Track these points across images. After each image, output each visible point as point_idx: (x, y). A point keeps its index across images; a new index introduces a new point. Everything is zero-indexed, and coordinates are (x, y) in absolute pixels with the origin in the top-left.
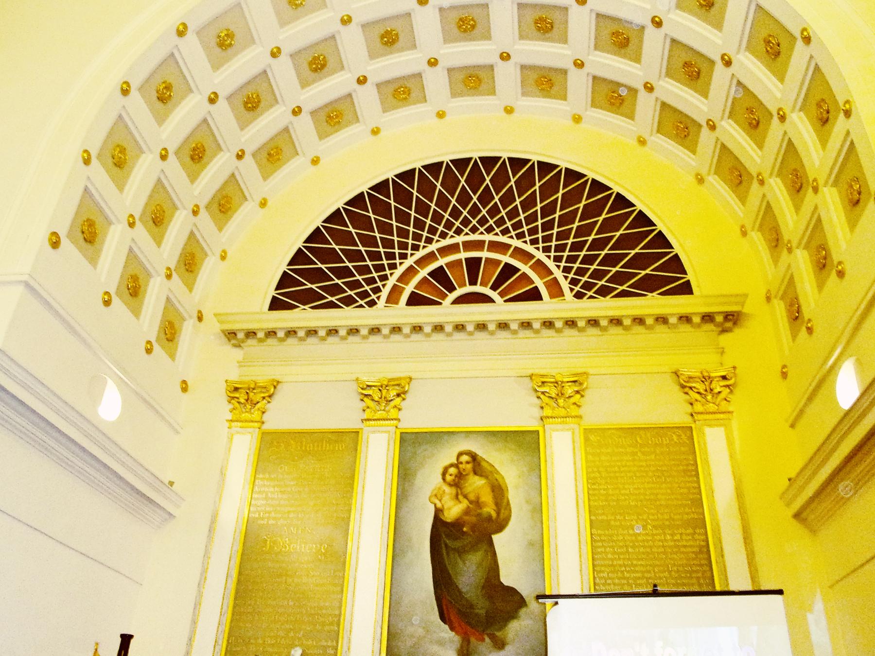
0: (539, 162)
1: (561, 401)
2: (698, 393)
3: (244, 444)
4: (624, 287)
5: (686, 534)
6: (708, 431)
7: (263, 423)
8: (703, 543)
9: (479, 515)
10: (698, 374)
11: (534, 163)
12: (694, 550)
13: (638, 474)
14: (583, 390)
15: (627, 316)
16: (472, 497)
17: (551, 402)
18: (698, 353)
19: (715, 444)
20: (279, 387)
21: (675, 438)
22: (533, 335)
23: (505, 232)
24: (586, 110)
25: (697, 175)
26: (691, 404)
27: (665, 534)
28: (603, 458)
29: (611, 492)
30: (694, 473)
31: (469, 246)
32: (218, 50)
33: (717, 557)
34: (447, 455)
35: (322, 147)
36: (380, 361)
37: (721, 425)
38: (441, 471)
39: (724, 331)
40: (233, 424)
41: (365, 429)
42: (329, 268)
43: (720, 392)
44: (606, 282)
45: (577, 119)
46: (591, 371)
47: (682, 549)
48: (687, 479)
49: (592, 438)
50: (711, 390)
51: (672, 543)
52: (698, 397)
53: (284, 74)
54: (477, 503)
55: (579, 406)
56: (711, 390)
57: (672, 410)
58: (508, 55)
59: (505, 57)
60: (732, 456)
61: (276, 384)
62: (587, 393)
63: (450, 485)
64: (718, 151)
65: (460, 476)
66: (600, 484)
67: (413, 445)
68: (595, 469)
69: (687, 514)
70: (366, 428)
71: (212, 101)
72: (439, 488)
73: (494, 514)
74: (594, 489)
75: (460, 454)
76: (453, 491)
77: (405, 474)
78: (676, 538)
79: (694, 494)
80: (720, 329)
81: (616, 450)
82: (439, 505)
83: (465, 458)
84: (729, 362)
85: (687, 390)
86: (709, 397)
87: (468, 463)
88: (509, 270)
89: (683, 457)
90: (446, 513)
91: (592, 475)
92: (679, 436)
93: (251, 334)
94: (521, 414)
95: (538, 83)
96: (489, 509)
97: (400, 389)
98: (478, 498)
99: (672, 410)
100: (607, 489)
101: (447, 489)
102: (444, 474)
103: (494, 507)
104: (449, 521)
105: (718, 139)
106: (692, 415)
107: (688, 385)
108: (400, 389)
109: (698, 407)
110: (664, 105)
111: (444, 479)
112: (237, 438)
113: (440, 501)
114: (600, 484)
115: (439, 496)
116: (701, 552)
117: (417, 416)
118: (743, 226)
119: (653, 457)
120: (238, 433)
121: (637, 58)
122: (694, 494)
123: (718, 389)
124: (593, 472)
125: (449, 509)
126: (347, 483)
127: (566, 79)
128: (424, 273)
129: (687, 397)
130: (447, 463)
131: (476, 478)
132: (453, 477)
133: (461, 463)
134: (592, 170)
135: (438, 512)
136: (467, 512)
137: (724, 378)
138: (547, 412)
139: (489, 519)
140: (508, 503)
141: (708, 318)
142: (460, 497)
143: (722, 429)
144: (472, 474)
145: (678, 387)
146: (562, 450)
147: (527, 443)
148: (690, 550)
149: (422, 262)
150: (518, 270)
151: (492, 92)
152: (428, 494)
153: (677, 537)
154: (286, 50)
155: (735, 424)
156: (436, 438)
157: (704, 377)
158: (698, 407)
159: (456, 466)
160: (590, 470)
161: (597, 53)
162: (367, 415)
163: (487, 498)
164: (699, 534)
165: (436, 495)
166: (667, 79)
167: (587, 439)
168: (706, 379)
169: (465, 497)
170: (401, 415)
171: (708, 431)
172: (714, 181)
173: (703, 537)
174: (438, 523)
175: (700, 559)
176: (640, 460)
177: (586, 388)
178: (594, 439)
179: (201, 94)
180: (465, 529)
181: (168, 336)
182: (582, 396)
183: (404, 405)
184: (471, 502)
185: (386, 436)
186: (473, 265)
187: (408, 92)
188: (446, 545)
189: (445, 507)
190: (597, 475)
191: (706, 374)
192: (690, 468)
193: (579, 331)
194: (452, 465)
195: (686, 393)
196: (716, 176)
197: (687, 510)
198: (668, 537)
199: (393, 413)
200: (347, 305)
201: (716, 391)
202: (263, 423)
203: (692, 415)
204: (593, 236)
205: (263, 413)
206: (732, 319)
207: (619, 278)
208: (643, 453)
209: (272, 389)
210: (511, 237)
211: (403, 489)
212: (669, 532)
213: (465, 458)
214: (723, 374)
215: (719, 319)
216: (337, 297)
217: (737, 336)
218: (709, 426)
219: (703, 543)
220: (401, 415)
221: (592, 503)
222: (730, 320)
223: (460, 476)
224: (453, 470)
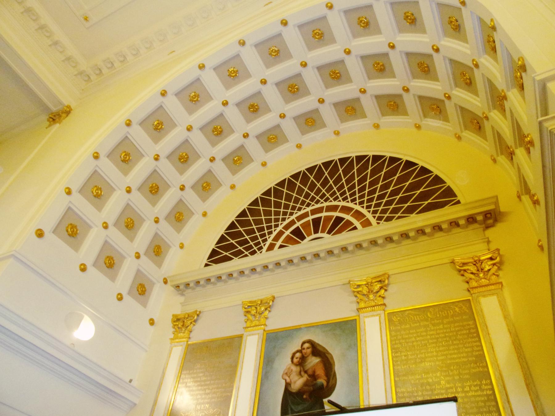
1: (371, 296)
2: (472, 273)
3: (178, 352)
6: (483, 300)
8: (490, 392)
9: (316, 384)
10: (471, 260)
12: (483, 399)
13: (430, 341)
14: (385, 286)
16: (310, 372)
17: (365, 299)
18: (470, 246)
19: (489, 307)
20: (201, 315)
21: (457, 309)
25: (456, 134)
26: (468, 282)
27: (456, 388)
28: (403, 332)
30: (475, 335)
31: (314, 212)
32: (155, 132)
33: (503, 403)
34: (295, 345)
35: (235, 179)
37: (493, 294)
39: (487, 227)
40: (173, 341)
41: (245, 334)
42: (235, 241)
43: (489, 270)
45: (377, 126)
46: (390, 273)
48: (470, 340)
49: (394, 319)
50: (482, 269)
52: (472, 276)
53: (199, 141)
54: (313, 376)
55: (384, 298)
56: (482, 269)
57: (453, 290)
58: (323, 100)
60: (506, 317)
62: (390, 288)
63: (296, 365)
64: (459, 112)
65: (303, 359)
66: (401, 352)
67: (273, 340)
68: (397, 342)
69: (474, 368)
71: (156, 159)
73: (325, 383)
74: (396, 357)
75: (304, 343)
78: (465, 390)
79: (478, 351)
81: (413, 325)
82: (288, 380)
85: (462, 272)
86: (481, 275)
87: (308, 348)
88: (339, 220)
89: (465, 323)
91: (396, 346)
92: (461, 308)
94: (342, 309)
95: (347, 111)
96: (322, 381)
97: (268, 305)
99: (453, 290)
102: (292, 358)
103: (326, 378)
104: (294, 391)
105: (455, 104)
106: (469, 291)
107: (462, 268)
108: (268, 305)
109: (474, 284)
110: (421, 98)
111: (292, 361)
112: (174, 349)
115: (288, 373)
116: (488, 400)
117: (277, 321)
118: (492, 156)
119: (441, 326)
120: (176, 346)
121: (393, 75)
122: (478, 351)
123: (487, 268)
124: (396, 344)
125: (295, 382)
127: (241, 60)
128: (288, 233)
130: (294, 350)
132: (298, 359)
133: (304, 349)
134: (388, 152)
135: (288, 385)
136: (306, 384)
137: (491, 259)
138: (362, 305)
139: (321, 387)
140: (335, 373)
141: (471, 220)
142: (303, 373)
145: (456, 273)
146: (373, 333)
147: (347, 329)
149: (286, 227)
150: (344, 219)
151: (324, 125)
152: (281, 372)
153: (467, 389)
154: (196, 126)
155: (506, 292)
156: (288, 333)
158: (474, 284)
159: (300, 351)
160: (394, 342)
161: (371, 81)
162: (248, 324)
163: (320, 372)
164: (486, 385)
165: (286, 373)
166: (414, 80)
167: (390, 321)
168: (477, 262)
169: (306, 372)
174: (288, 393)
175: (489, 406)
176: (431, 330)
177: (388, 284)
178: (396, 321)
180: (305, 397)
181: (140, 292)
182: (386, 290)
184: (309, 376)
185: (257, 336)
186: (316, 222)
187: (276, 137)
188: (292, 409)
189: (292, 381)
191: (476, 259)
192: (472, 331)
194: (298, 351)
195: (463, 275)
196: (467, 131)
197: (472, 365)
198: (459, 390)
199: (263, 321)
200: (236, 257)
201: (486, 269)
202: (190, 338)
204: (368, 181)
205: (191, 332)
208: (434, 325)
209: (196, 317)
212: (460, 385)
213: (306, 345)
214: (489, 256)
215: (480, 218)
217: (500, 227)
218: (484, 296)
219: (490, 392)
221: (396, 368)
222: (490, 218)
223: (303, 359)
224: (298, 355)
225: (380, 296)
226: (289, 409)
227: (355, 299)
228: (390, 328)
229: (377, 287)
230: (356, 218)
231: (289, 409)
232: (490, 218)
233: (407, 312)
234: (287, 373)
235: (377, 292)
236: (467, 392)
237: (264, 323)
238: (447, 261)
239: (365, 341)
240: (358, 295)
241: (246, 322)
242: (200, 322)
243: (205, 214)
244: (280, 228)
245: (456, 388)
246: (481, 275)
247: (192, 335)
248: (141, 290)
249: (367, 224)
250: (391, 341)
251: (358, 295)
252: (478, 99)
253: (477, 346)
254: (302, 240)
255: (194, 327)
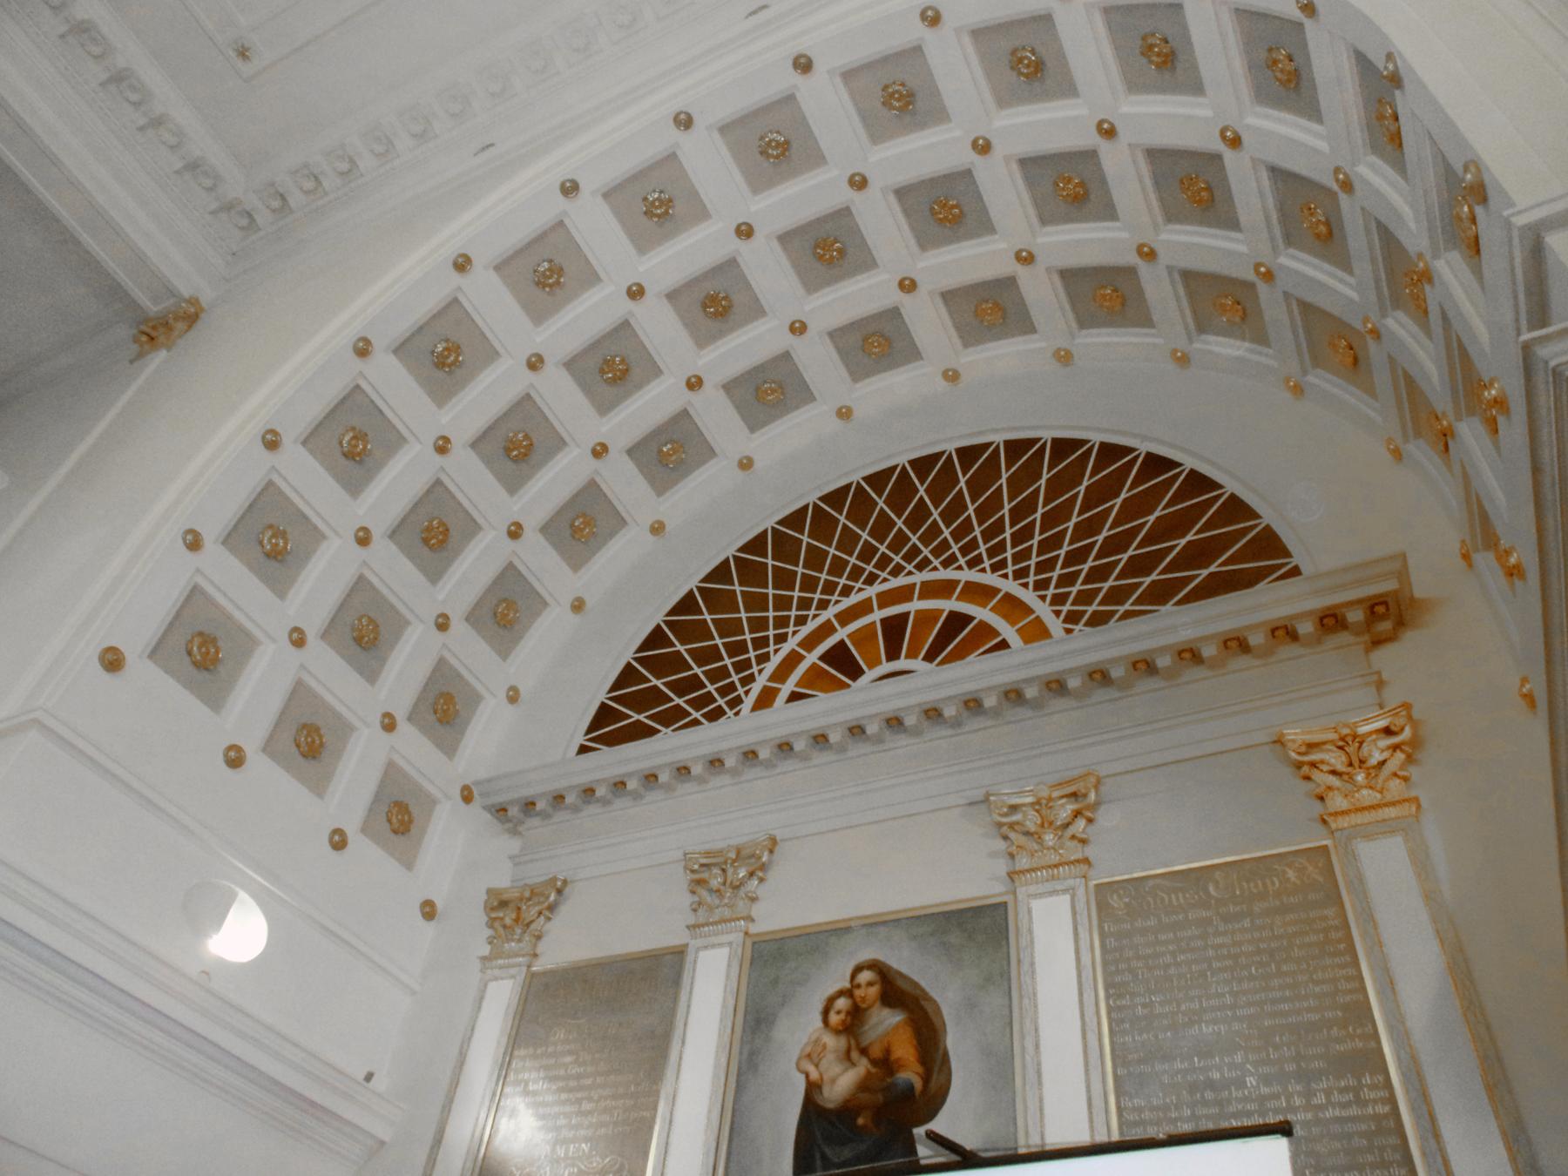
0: (912, 462)
1: (1049, 838)
2: (1334, 772)
3: (502, 995)
4: (1127, 607)
5: (1342, 1091)
6: (1364, 849)
7: (535, 955)
11: (904, 468)
15: (1162, 650)
16: (876, 1052)
18: (1325, 698)
19: (1385, 872)
21: (1291, 874)
22: (1030, 713)
23: (897, 571)
24: (1073, 336)
26: (1322, 799)
27: (1289, 1097)
28: (1138, 939)
29: (1158, 1010)
30: (1342, 946)
31: (886, 599)
36: (720, 817)
38: (819, 1006)
39: (1377, 642)
41: (694, 943)
42: (666, 681)
43: (1383, 763)
44: (1085, 612)
46: (1103, 770)
47: (1336, 1128)
49: (1115, 901)
50: (1362, 762)
51: (1309, 1116)
52: (1334, 781)
54: (886, 1064)
55: (1083, 842)
56: (1362, 762)
59: (695, 384)
61: (773, 844)
63: (837, 1032)
65: (857, 1014)
66: (1133, 995)
67: (771, 963)
68: (1122, 966)
70: (694, 943)
72: (817, 1041)
73: (918, 1084)
74: (1120, 1008)
75: (858, 969)
76: (842, 1042)
77: (754, 1022)
79: (1351, 992)
80: (1367, 638)
82: (814, 1075)
83: (866, 976)
84: (1393, 698)
86: (1360, 778)
87: (870, 984)
90: (826, 1091)
91: (1118, 979)
93: (529, 805)
94: (962, 872)
96: (910, 1075)
98: (888, 1051)
100: (1150, 1005)
101: (830, 1040)
103: (920, 1069)
104: (830, 1106)
105: (1286, 295)
106: (1324, 822)
109: (1338, 802)
111: (826, 1021)
112: (492, 986)
113: (817, 1066)
114: (1133, 995)
115: (814, 1056)
117: (782, 906)
118: (1389, 441)
119: (1247, 923)
120: (496, 979)
122: (1351, 992)
123: (1377, 757)
124: (1118, 972)
125: (833, 1081)
126: (654, 1053)
128: (812, 658)
129: (1310, 785)
130: (832, 990)
131: (886, 1012)
132: (842, 1016)
133: (859, 986)
135: (813, 1088)
136: (863, 1086)
137: (1388, 731)
138: (1023, 862)
141: (1331, 621)
142: (855, 1055)
143: (1398, 840)
144: (878, 1004)
146: (1055, 943)
147: (982, 929)
148: (1350, 1127)
149: (809, 643)
150: (971, 618)
152: (795, 1053)
153: (1320, 1099)
156: (814, 942)
157: (1342, 739)
158: (1338, 802)
159: (848, 993)
161: (1049, 229)
162: (702, 916)
163: (905, 1050)
164: (1373, 1087)
165: (809, 1056)
167: (1103, 906)
169: (864, 1052)
170: (1089, 851)
171: (1364, 849)
172: (1318, 380)
173: (1384, 1094)
175: (1382, 1149)
179: (578, 446)
180: (860, 1121)
183: (762, 891)
184: (874, 1062)
185: (725, 951)
189: (825, 1077)
190: (1128, 977)
192: (1333, 935)
193: (952, 727)
194: (841, 993)
195: (1307, 778)
196: (1319, 371)
198: (1298, 1101)
201: (1374, 761)
203: (1324, 822)
206: (1385, 615)
207: (1116, 596)
208: (1226, 919)
209: (552, 897)
210: (910, 573)
211: (752, 1054)
213: (866, 976)
214: (1381, 724)
215: (1355, 616)
216: (1087, 617)
218: (1368, 837)
219: (1383, 1109)
220: (1089, 851)
222: (1383, 617)
223: (857, 1014)
224: (842, 1003)
225: (1073, 837)
226: (818, 1156)
227: (1001, 845)
228: (1101, 928)
229: (1065, 810)
230: (1005, 617)
231: (818, 1156)
232: (1385, 615)
233: (1151, 883)
234: (812, 1055)
235: (1066, 826)
236: (1320, 1107)
237: (744, 914)
238: (1262, 737)
239: (1032, 964)
240: (1012, 835)
241: (695, 910)
242: (564, 910)
243: (578, 606)
244: (791, 644)
245: (1289, 1097)
246: (1360, 778)
247: (541, 948)
248: (399, 817)
249: (1036, 632)
250: (1105, 963)
251: (1012, 835)
252: (1351, 280)
253: (1348, 979)
254: (854, 679)
255: (549, 925)
